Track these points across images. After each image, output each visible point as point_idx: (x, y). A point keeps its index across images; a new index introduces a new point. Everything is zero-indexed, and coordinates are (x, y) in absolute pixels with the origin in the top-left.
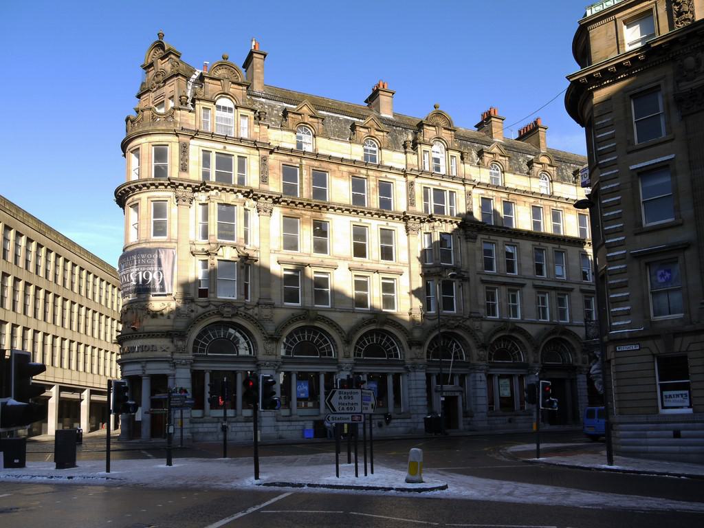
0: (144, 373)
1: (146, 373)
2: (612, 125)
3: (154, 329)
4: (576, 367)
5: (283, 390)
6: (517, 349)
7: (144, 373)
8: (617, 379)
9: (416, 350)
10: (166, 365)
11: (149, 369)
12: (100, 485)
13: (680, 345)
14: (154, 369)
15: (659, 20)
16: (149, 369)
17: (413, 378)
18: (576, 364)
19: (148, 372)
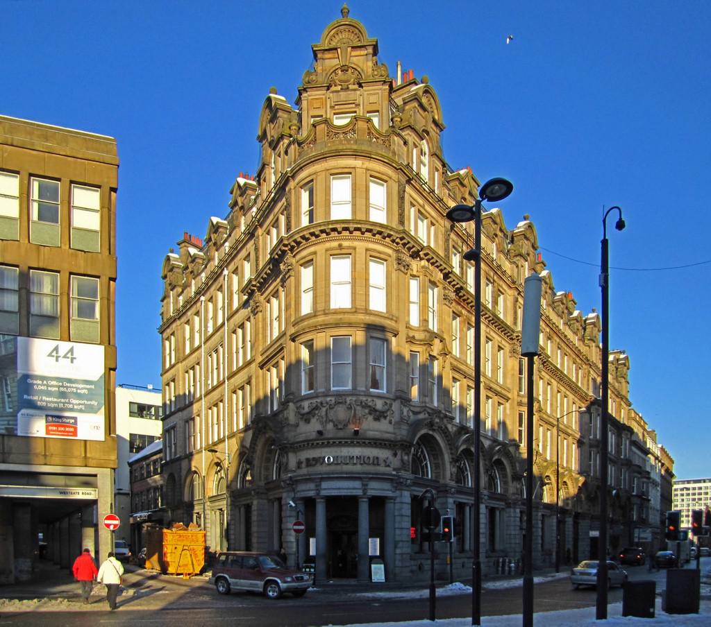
0: (318, 494)
1: (322, 494)
2: (109, 344)
3: (376, 435)
4: (567, 510)
5: (652, 610)
6: (425, 459)
7: (318, 494)
8: (258, 537)
9: (546, 474)
10: (387, 486)
11: (325, 489)
12: (408, 102)
13: (355, 437)
14: (376, 489)
15: (108, 339)
16: (325, 489)
17: (517, 536)
18: (567, 508)
19: (323, 493)
